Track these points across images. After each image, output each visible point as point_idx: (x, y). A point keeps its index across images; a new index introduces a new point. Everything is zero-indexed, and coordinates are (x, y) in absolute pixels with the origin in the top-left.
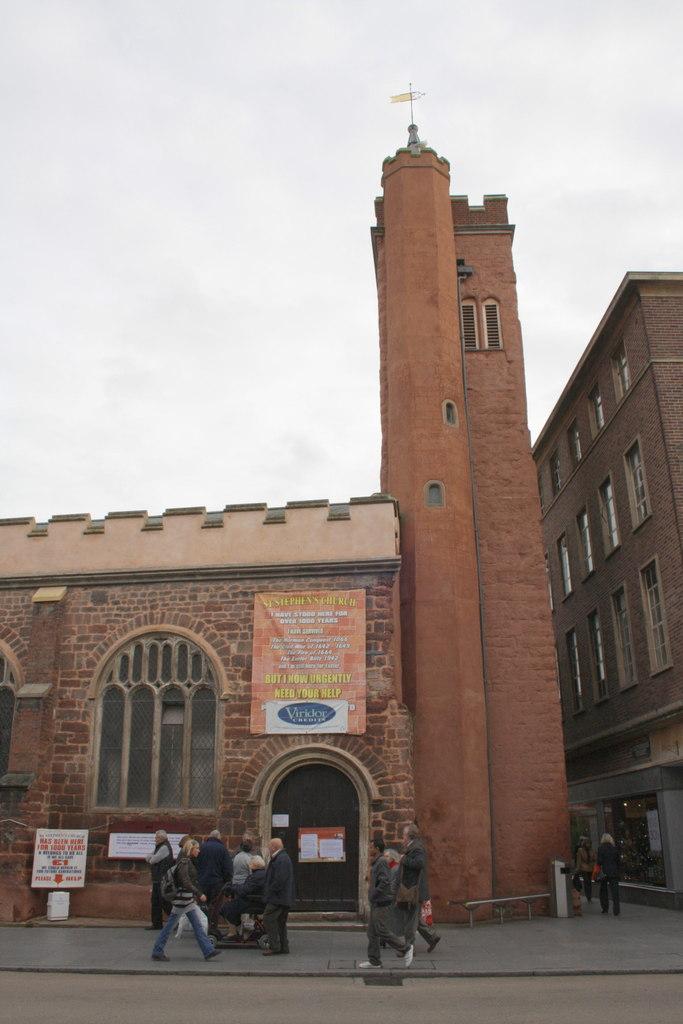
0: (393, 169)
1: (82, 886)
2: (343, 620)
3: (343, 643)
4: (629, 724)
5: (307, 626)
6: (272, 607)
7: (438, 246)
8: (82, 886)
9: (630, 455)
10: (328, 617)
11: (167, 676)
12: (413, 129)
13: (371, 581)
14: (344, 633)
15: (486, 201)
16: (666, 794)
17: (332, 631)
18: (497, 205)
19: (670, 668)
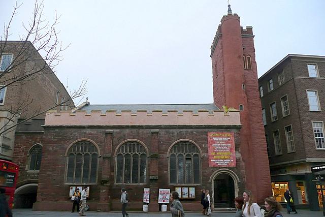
0: (225, 19)
1: (160, 189)
2: (229, 140)
3: (229, 145)
4: (279, 164)
5: (220, 141)
6: (212, 136)
7: (233, 41)
8: (160, 189)
9: (271, 105)
10: (226, 139)
11: (134, 152)
12: (229, 6)
13: (235, 131)
14: (229, 143)
15: (247, 28)
16: (291, 181)
17: (227, 142)
18: (250, 30)
19: (281, 155)
